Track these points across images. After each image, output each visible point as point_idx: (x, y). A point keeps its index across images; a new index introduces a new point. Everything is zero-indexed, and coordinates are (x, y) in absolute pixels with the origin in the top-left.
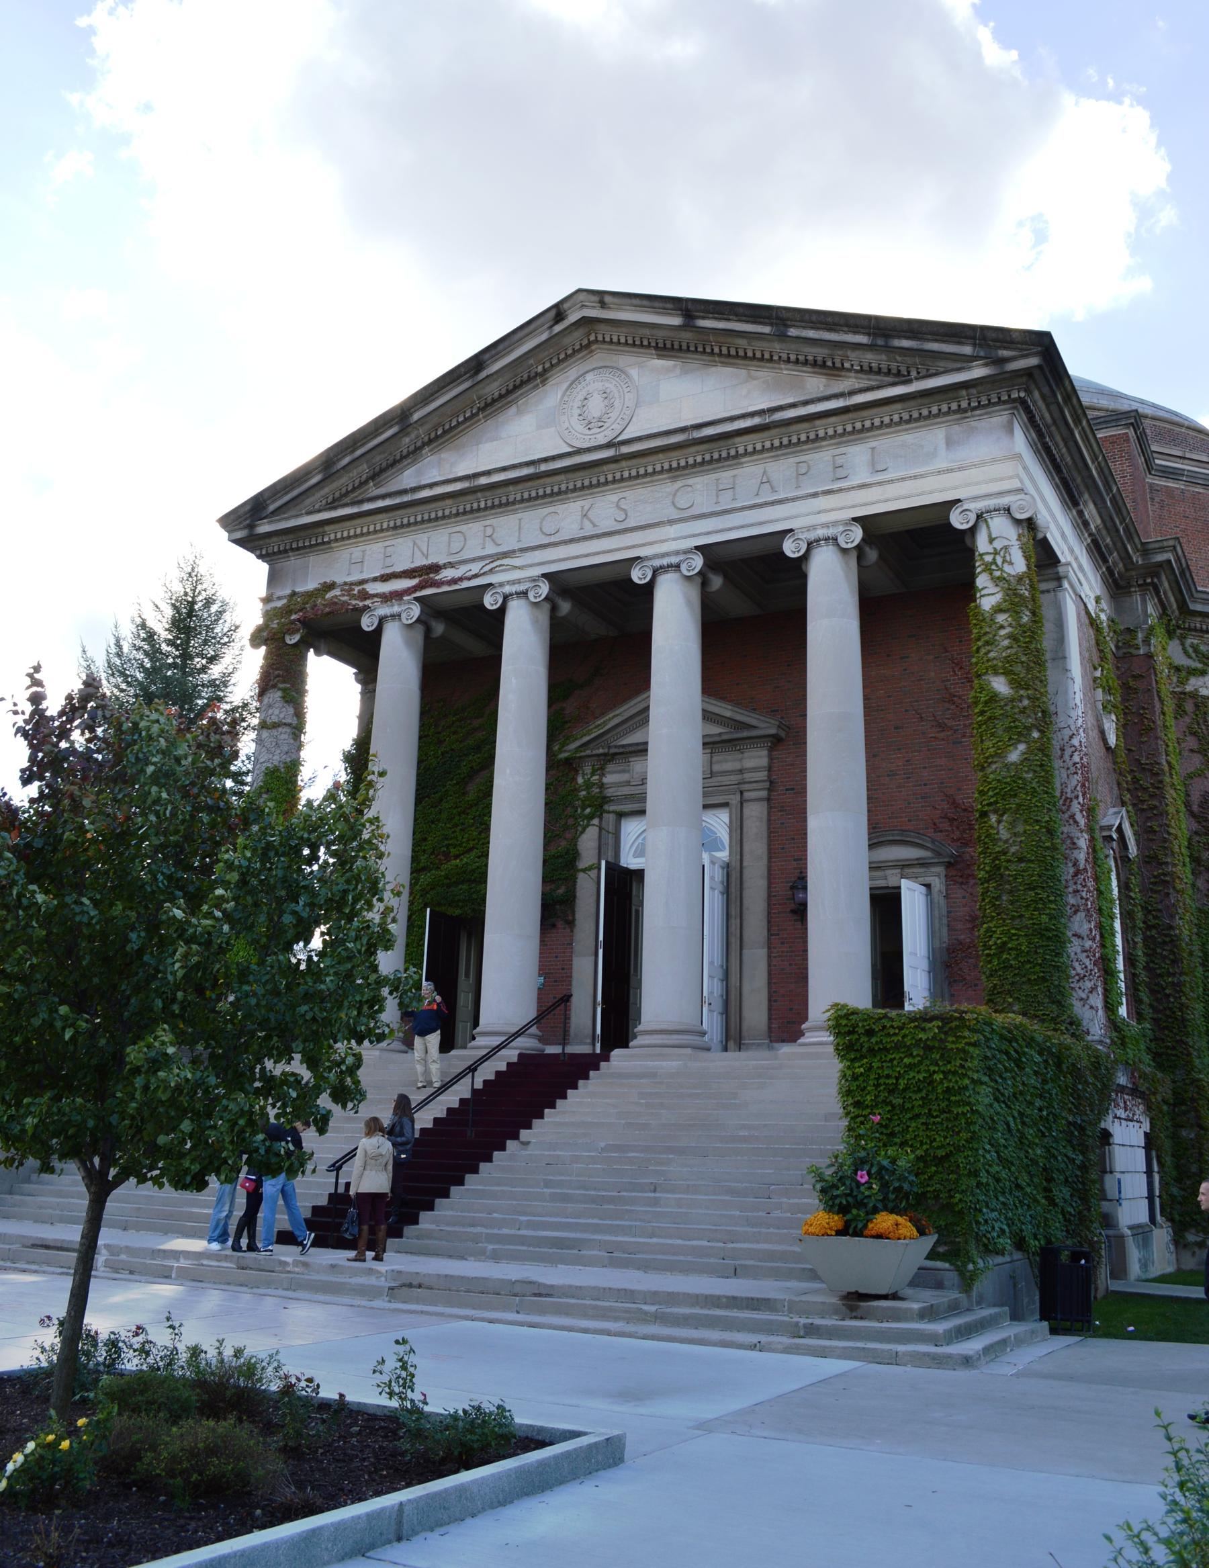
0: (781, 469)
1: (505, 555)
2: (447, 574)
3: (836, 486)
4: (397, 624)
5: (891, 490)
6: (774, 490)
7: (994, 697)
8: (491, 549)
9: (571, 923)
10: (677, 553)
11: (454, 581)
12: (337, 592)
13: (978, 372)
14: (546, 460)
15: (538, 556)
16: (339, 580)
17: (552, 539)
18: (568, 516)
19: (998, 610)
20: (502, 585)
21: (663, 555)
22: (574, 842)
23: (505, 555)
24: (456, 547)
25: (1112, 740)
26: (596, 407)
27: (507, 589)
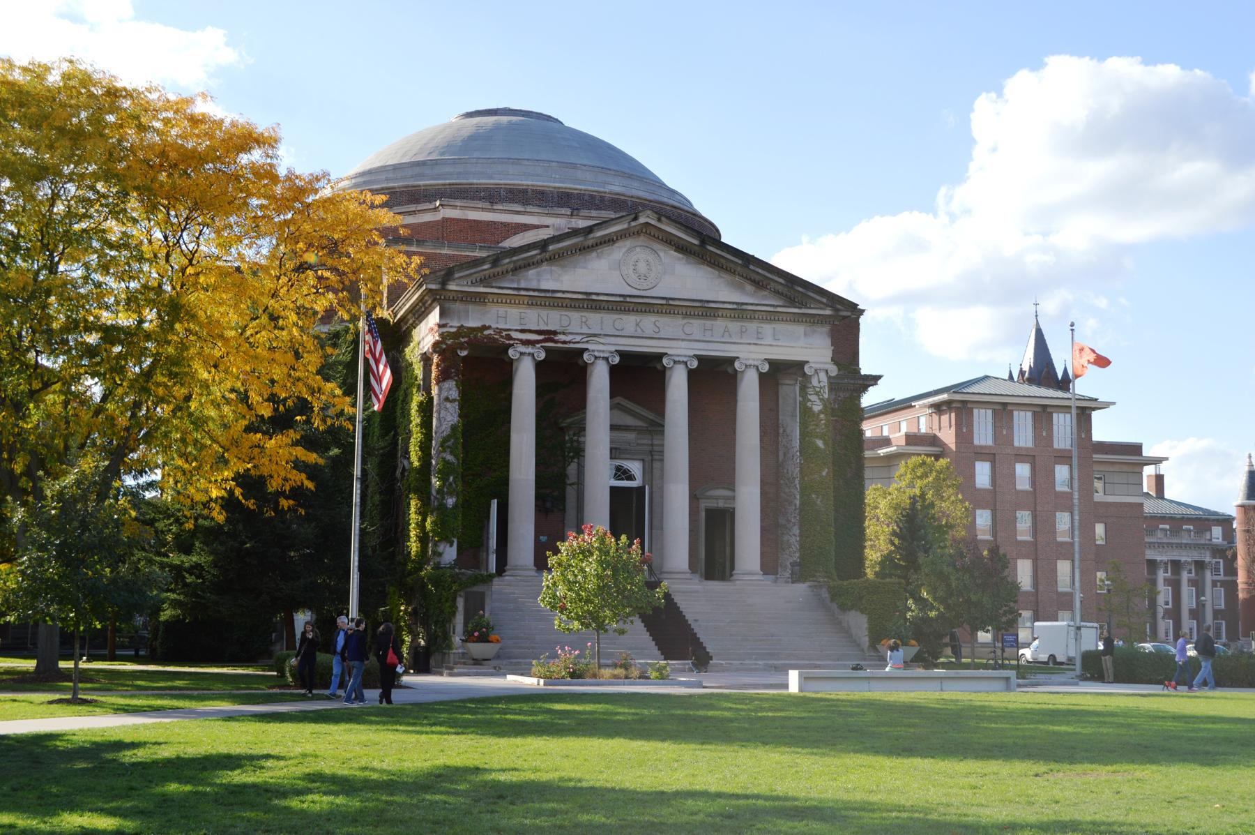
0: (734, 326)
1: (595, 335)
2: (561, 337)
7: (818, 448)
8: (585, 330)
9: (564, 510)
11: (564, 342)
12: (491, 332)
13: (828, 312)
15: (612, 340)
16: (494, 326)
18: (629, 322)
19: (821, 412)
22: (564, 468)
23: (595, 335)
24: (565, 323)
27: (597, 354)
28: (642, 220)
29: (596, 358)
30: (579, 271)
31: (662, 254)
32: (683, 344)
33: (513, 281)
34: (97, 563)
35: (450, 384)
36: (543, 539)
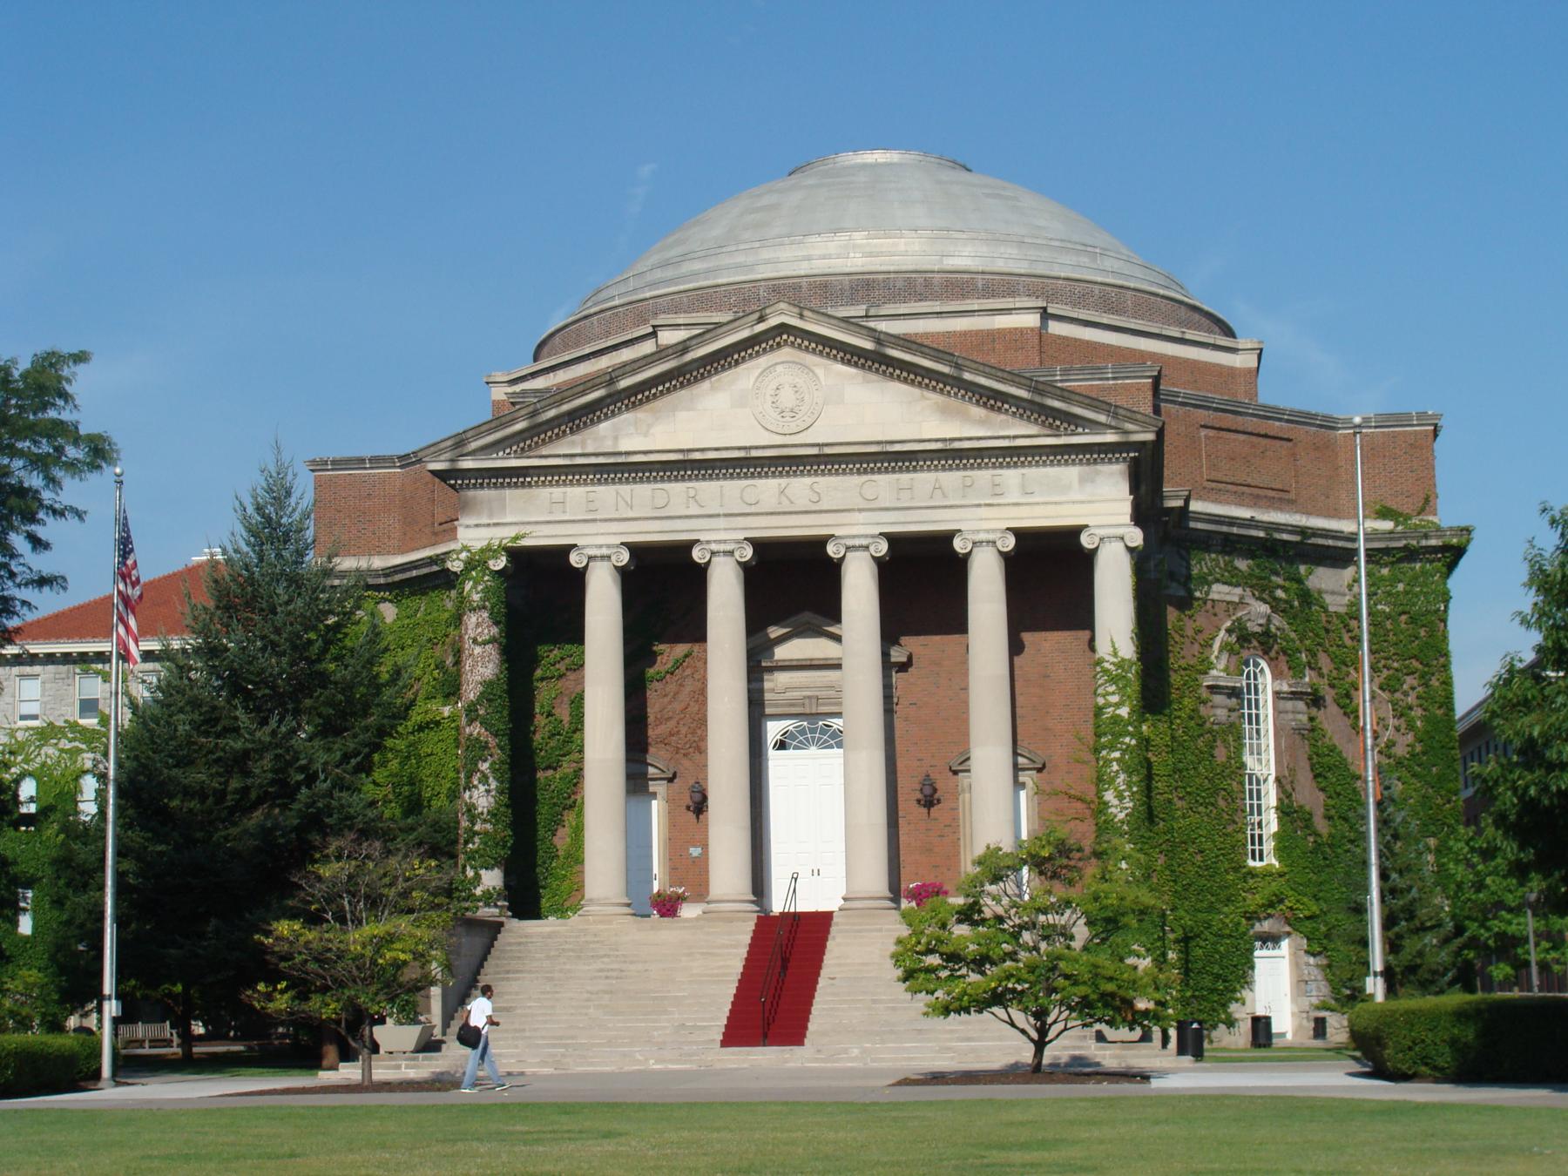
0: (951, 479)
3: (995, 501)
4: (605, 564)
5: (1038, 511)
6: (944, 496)
10: (866, 536)
14: (757, 448)
15: (741, 522)
17: (753, 509)
18: (767, 489)
20: (708, 542)
21: (854, 537)
25: (1024, 836)
26: (787, 398)
27: (714, 547)
28: (773, 321)
29: (713, 553)
30: (682, 415)
31: (820, 372)
32: (861, 517)
33: (573, 444)
34: (1129, 734)
35: (1336, 604)
36: (695, 852)
